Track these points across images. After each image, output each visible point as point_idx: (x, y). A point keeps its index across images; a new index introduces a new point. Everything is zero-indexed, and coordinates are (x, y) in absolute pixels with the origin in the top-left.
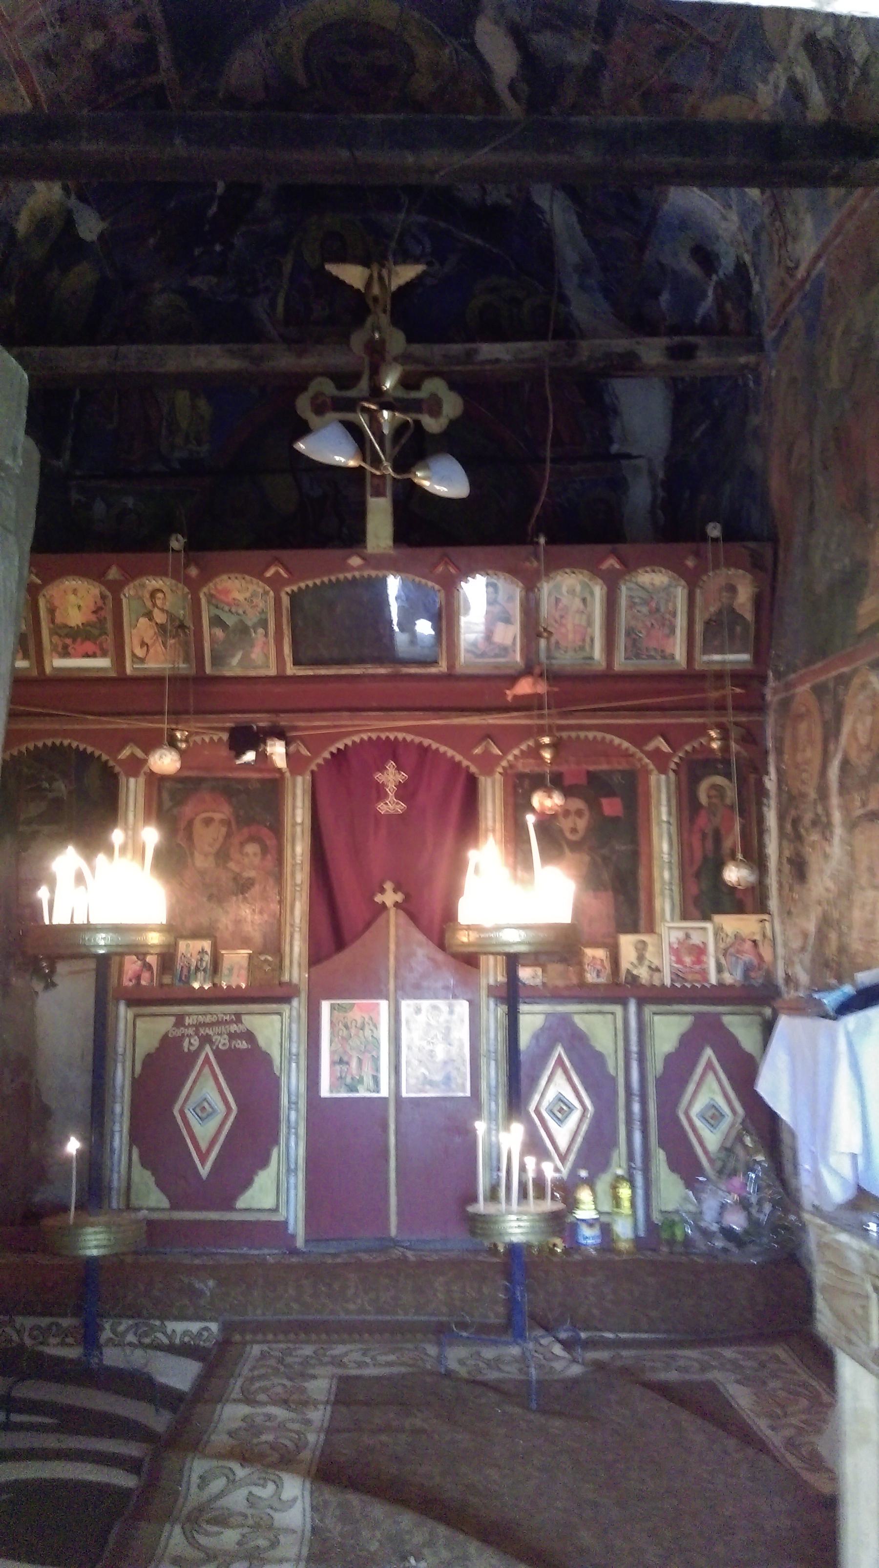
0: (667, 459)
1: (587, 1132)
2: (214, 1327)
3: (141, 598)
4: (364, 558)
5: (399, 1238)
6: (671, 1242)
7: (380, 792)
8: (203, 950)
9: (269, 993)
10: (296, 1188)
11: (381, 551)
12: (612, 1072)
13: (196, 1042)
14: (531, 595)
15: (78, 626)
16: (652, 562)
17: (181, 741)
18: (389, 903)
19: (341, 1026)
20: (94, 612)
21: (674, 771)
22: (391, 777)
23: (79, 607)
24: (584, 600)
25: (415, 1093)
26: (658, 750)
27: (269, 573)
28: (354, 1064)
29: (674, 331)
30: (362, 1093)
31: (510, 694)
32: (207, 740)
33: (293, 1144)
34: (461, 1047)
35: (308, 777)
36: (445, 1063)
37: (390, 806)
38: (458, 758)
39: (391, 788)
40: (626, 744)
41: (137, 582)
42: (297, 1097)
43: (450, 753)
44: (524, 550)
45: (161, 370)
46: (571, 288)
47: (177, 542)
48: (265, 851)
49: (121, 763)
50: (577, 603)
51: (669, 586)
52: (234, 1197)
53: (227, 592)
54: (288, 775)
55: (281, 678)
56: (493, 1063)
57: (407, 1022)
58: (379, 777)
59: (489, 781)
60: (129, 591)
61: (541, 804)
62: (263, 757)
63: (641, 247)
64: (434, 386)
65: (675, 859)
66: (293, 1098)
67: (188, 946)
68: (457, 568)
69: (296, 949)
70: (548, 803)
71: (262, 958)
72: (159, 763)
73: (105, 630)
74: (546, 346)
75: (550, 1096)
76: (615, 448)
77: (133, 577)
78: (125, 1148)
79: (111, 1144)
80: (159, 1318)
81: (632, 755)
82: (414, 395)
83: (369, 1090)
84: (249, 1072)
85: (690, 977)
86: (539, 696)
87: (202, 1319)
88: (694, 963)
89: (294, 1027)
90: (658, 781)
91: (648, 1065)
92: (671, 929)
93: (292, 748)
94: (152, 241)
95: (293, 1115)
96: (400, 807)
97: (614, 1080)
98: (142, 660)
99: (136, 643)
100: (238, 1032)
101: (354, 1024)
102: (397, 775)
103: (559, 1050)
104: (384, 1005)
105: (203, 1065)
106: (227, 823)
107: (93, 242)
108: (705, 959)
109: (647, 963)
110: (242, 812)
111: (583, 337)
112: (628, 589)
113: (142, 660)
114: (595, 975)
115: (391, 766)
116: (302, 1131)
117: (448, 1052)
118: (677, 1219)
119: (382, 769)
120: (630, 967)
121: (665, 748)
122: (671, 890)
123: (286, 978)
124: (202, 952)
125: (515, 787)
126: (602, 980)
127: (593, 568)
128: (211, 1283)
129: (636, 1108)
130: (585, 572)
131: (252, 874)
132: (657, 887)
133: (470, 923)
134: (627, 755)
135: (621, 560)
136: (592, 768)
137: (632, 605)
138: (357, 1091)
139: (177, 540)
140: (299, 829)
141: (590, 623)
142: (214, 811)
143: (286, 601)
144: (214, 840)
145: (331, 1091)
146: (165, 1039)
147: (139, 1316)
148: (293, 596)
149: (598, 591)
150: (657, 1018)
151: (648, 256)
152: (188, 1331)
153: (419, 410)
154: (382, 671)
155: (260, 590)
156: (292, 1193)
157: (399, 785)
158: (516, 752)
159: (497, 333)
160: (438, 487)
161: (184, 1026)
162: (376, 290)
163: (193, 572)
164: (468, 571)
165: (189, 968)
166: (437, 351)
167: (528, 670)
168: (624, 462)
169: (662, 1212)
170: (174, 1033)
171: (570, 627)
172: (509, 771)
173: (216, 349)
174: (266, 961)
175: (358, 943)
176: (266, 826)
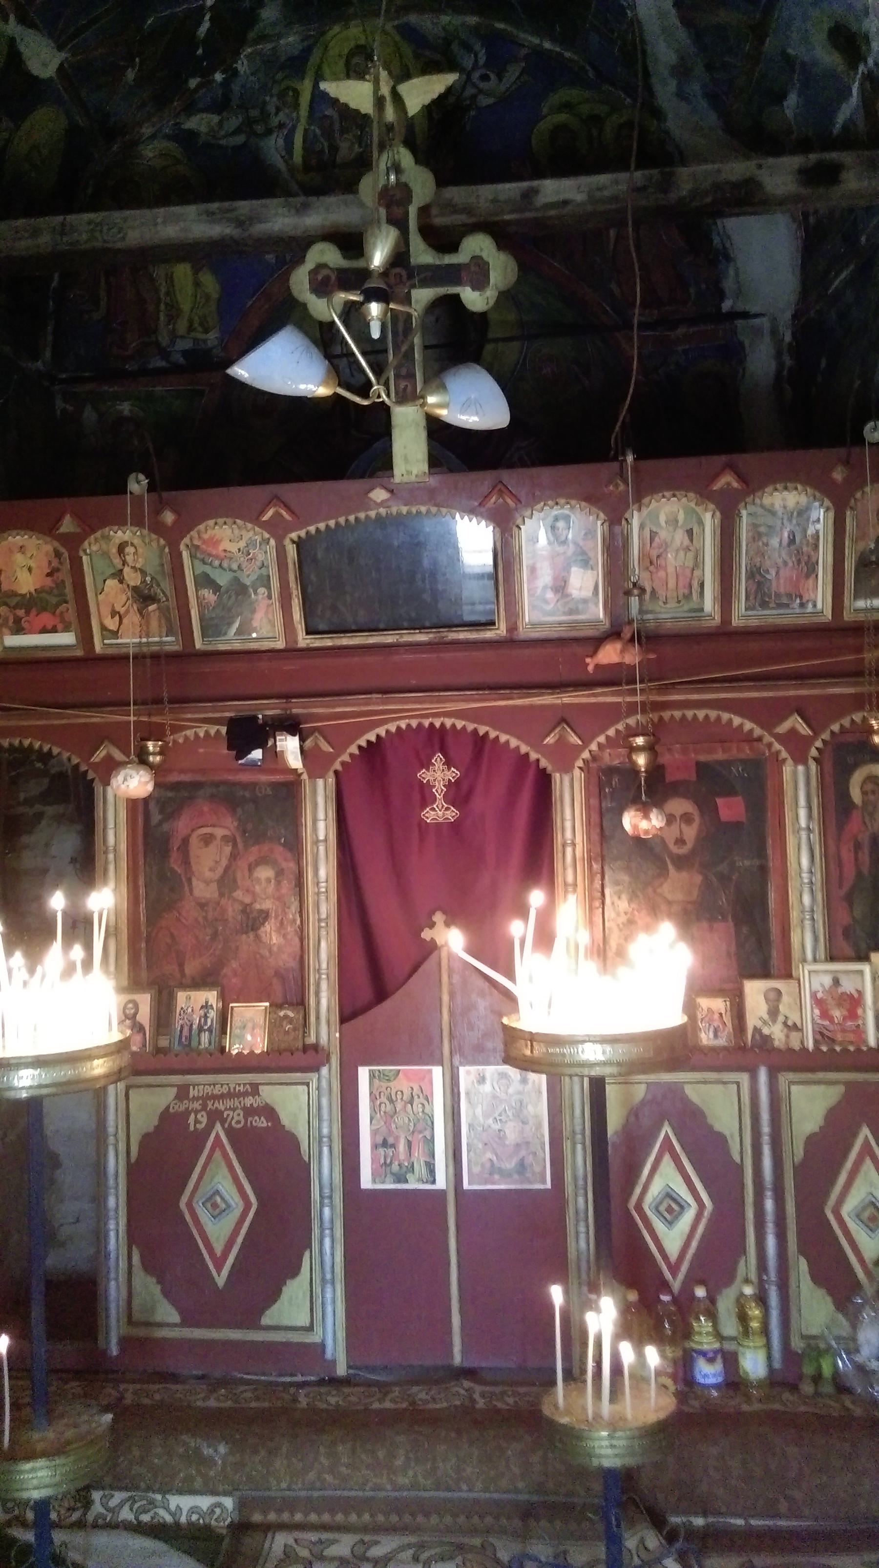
0: (795, 317)
1: (703, 1236)
2: (228, 1502)
3: (106, 555)
4: (391, 491)
5: (466, 1365)
6: (817, 1378)
7: (425, 796)
8: (207, 1002)
9: (293, 1056)
10: (334, 1301)
11: (413, 478)
12: (736, 1158)
13: (203, 1119)
14: (617, 529)
17: (154, 754)
19: (384, 1099)
20: (48, 575)
21: (815, 759)
23: (30, 569)
24: (690, 533)
25: (480, 1184)
26: (793, 731)
28: (402, 1147)
29: (804, 146)
30: (413, 1185)
32: (202, 735)
33: (328, 1247)
34: (539, 1126)
35: (331, 780)
36: (518, 1146)
37: (439, 812)
38: (524, 749)
39: (439, 790)
40: (748, 725)
41: (98, 534)
43: (514, 743)
45: (119, 245)
46: (665, 92)
47: (137, 484)
48: (280, 873)
49: (95, 766)
50: (680, 537)
52: (261, 1312)
53: (215, 543)
54: (305, 776)
55: (292, 652)
56: (579, 1147)
57: (467, 1094)
58: (425, 776)
59: (567, 779)
60: (91, 547)
61: (635, 827)
62: (275, 756)
63: (760, 32)
64: (478, 245)
65: (818, 878)
66: (327, 1191)
67: (189, 998)
69: (324, 1002)
70: (644, 825)
71: (282, 1014)
72: (123, 787)
73: (66, 595)
74: (639, 176)
75: (656, 1189)
77: (93, 531)
78: (124, 1250)
79: (106, 1248)
80: (160, 1491)
81: (760, 739)
82: (450, 259)
83: (420, 1180)
84: (272, 1158)
85: (839, 1037)
87: (214, 1493)
88: (845, 1018)
89: (325, 1102)
90: (795, 774)
92: (815, 976)
93: (309, 743)
94: (130, 75)
96: (452, 814)
97: (740, 1169)
98: (115, 634)
99: (106, 611)
101: (399, 1097)
102: (446, 772)
103: (666, 1129)
104: (437, 1072)
105: (213, 1150)
106: (230, 840)
107: (51, 79)
108: (860, 1011)
109: (781, 1019)
111: (684, 162)
112: (749, 514)
113: (115, 634)
114: (711, 1035)
115: (438, 759)
116: (339, 1232)
117: (522, 1132)
118: (822, 1346)
119: (426, 764)
120: (759, 1024)
121: (804, 729)
122: (813, 919)
124: (206, 1006)
126: (722, 1042)
127: (703, 490)
128: (222, 1449)
129: (769, 1205)
130: (691, 495)
131: (267, 905)
132: (794, 915)
133: (534, 1031)
134: (750, 739)
135: (741, 477)
136: (702, 758)
138: (406, 1181)
139: (138, 482)
140: (322, 848)
141: (698, 563)
142: (213, 826)
143: (291, 551)
144: (217, 862)
145: (374, 1181)
146: (166, 1116)
147: (137, 1488)
148: (299, 544)
149: (710, 520)
150: (794, 1088)
152: (197, 1507)
153: (458, 282)
154: (422, 637)
155: (258, 538)
156: (329, 1309)
157: (449, 785)
158: (602, 739)
159: (566, 164)
160: (464, 418)
161: (187, 1098)
163: (169, 517)
164: (532, 501)
165: (191, 1025)
166: (487, 195)
167: (614, 634)
168: (740, 323)
169: (803, 1337)
170: (176, 1107)
172: (593, 765)
173: (191, 210)
174: (286, 1017)
175: (401, 991)
176: (281, 844)
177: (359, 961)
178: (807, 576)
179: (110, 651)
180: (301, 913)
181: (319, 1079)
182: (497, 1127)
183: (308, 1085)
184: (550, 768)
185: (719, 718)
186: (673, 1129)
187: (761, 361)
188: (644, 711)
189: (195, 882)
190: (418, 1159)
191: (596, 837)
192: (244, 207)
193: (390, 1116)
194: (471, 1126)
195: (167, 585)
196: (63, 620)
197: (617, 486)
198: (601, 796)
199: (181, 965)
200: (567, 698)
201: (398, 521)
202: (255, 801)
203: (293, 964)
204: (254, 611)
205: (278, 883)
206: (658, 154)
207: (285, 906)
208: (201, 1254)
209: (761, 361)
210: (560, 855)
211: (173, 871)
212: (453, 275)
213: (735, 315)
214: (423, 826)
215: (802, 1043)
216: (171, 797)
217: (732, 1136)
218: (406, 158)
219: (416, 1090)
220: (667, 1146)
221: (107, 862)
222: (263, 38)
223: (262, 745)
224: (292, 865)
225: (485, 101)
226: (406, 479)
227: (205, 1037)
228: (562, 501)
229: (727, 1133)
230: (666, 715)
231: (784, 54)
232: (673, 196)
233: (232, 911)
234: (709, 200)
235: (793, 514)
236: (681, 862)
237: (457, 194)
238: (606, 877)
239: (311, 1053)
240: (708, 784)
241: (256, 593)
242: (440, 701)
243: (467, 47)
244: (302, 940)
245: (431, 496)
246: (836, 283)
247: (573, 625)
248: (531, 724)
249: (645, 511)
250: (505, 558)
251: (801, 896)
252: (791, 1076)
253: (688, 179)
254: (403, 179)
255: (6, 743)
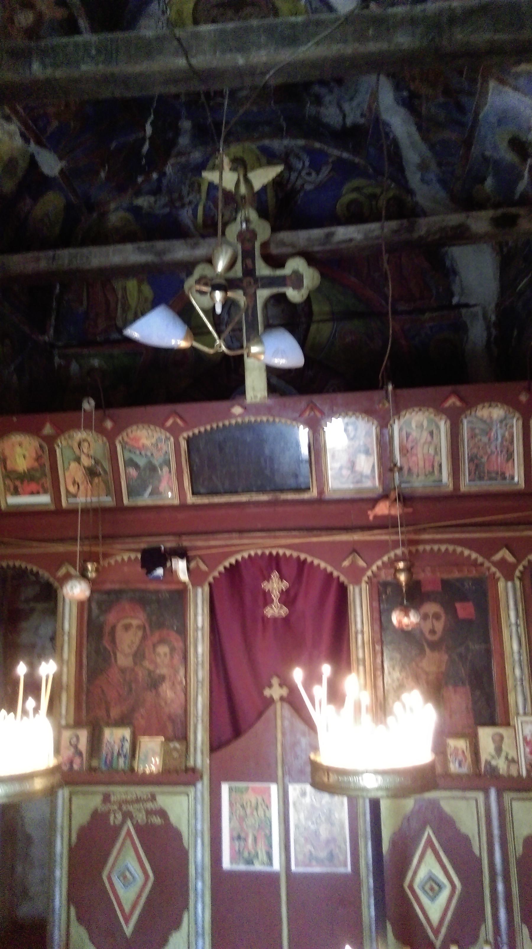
0: (497, 305)
7: (267, 599)
9: (178, 775)
11: (258, 400)
13: (119, 817)
14: (386, 431)
15: (24, 471)
16: (491, 399)
18: (276, 697)
19: (238, 806)
22: (275, 585)
23: (24, 457)
24: (431, 433)
27: (169, 423)
28: (250, 840)
29: (496, 206)
30: (258, 867)
31: (371, 515)
33: (200, 910)
34: (342, 827)
35: (207, 588)
37: (276, 610)
38: (329, 569)
39: (275, 595)
40: (474, 555)
42: (203, 869)
43: (323, 565)
44: (377, 395)
46: (414, 179)
47: (89, 405)
48: (173, 649)
50: (425, 434)
51: (505, 418)
54: (190, 586)
55: (183, 507)
57: (294, 804)
58: (266, 586)
60: (62, 445)
61: (400, 622)
62: (171, 573)
63: (468, 143)
64: (296, 264)
66: (200, 870)
68: (322, 413)
70: (405, 621)
73: (45, 473)
74: (393, 224)
75: (422, 874)
76: (455, 300)
81: (482, 565)
82: (279, 272)
83: (263, 863)
84: (163, 846)
86: (394, 518)
89: (199, 808)
91: (511, 847)
93: (193, 565)
94: (103, 175)
95: (200, 885)
96: (284, 611)
97: (479, 860)
100: (154, 809)
101: (249, 804)
103: (429, 832)
104: (274, 788)
105: (124, 839)
107: (55, 179)
109: (503, 754)
110: (154, 618)
112: (469, 422)
113: (75, 496)
115: (275, 576)
119: (268, 578)
120: (489, 758)
121: (510, 558)
123: (191, 763)
124: (123, 739)
125: (380, 595)
126: (464, 770)
127: (439, 408)
129: (500, 887)
130: (431, 410)
132: (510, 683)
134: (475, 564)
135: (461, 399)
136: (445, 576)
137: (473, 436)
140: (200, 634)
141: (438, 451)
142: (132, 617)
143: (183, 445)
148: (189, 441)
151: (475, 150)
154: (264, 497)
155: (163, 437)
157: (282, 592)
158: (379, 563)
162: (243, 190)
164: (333, 413)
165: (113, 753)
166: (303, 237)
167: (385, 496)
168: (464, 311)
171: (420, 456)
173: (129, 247)
174: (175, 749)
175: (253, 730)
177: (224, 708)
178: (508, 460)
179: (71, 507)
180: (186, 677)
181: (196, 792)
182: (313, 827)
183: (188, 795)
184: (346, 582)
185: (454, 551)
186: (434, 833)
187: (477, 333)
188: (403, 545)
189: (118, 655)
190: (261, 850)
191: (377, 628)
192: (160, 245)
193: (242, 819)
194: (297, 827)
195: (107, 465)
196: (43, 486)
197: (384, 405)
198: (380, 601)
199: (108, 711)
200: (357, 537)
201: (250, 426)
202: (158, 601)
203: (180, 712)
204: (160, 481)
205: (172, 657)
206: (403, 209)
207: (176, 672)
208: (116, 911)
209: (477, 333)
210: (354, 640)
211: (105, 649)
212: (282, 281)
213: (460, 306)
214: (264, 618)
215: (519, 773)
216: (104, 598)
217: (473, 836)
218: (253, 215)
219: (260, 800)
220: (429, 842)
221: (63, 641)
222: (180, 154)
223: (164, 565)
224: (181, 644)
225: (308, 187)
226: (253, 400)
227: (121, 761)
228: (350, 413)
229: (470, 836)
230: (421, 548)
231: (483, 156)
232: (416, 235)
233: (141, 674)
234: (437, 237)
235: (495, 419)
236: (434, 646)
237: (285, 236)
238: (385, 654)
239: (190, 773)
240: (450, 593)
241: (161, 470)
242: (275, 537)
243: (299, 158)
244: (186, 694)
245: (269, 410)
246: (521, 286)
247: (359, 490)
248: (335, 553)
249: (402, 420)
250: (317, 447)
251: (514, 669)
252: (512, 795)
253: (424, 226)
254: (252, 226)
255: (4, 564)
